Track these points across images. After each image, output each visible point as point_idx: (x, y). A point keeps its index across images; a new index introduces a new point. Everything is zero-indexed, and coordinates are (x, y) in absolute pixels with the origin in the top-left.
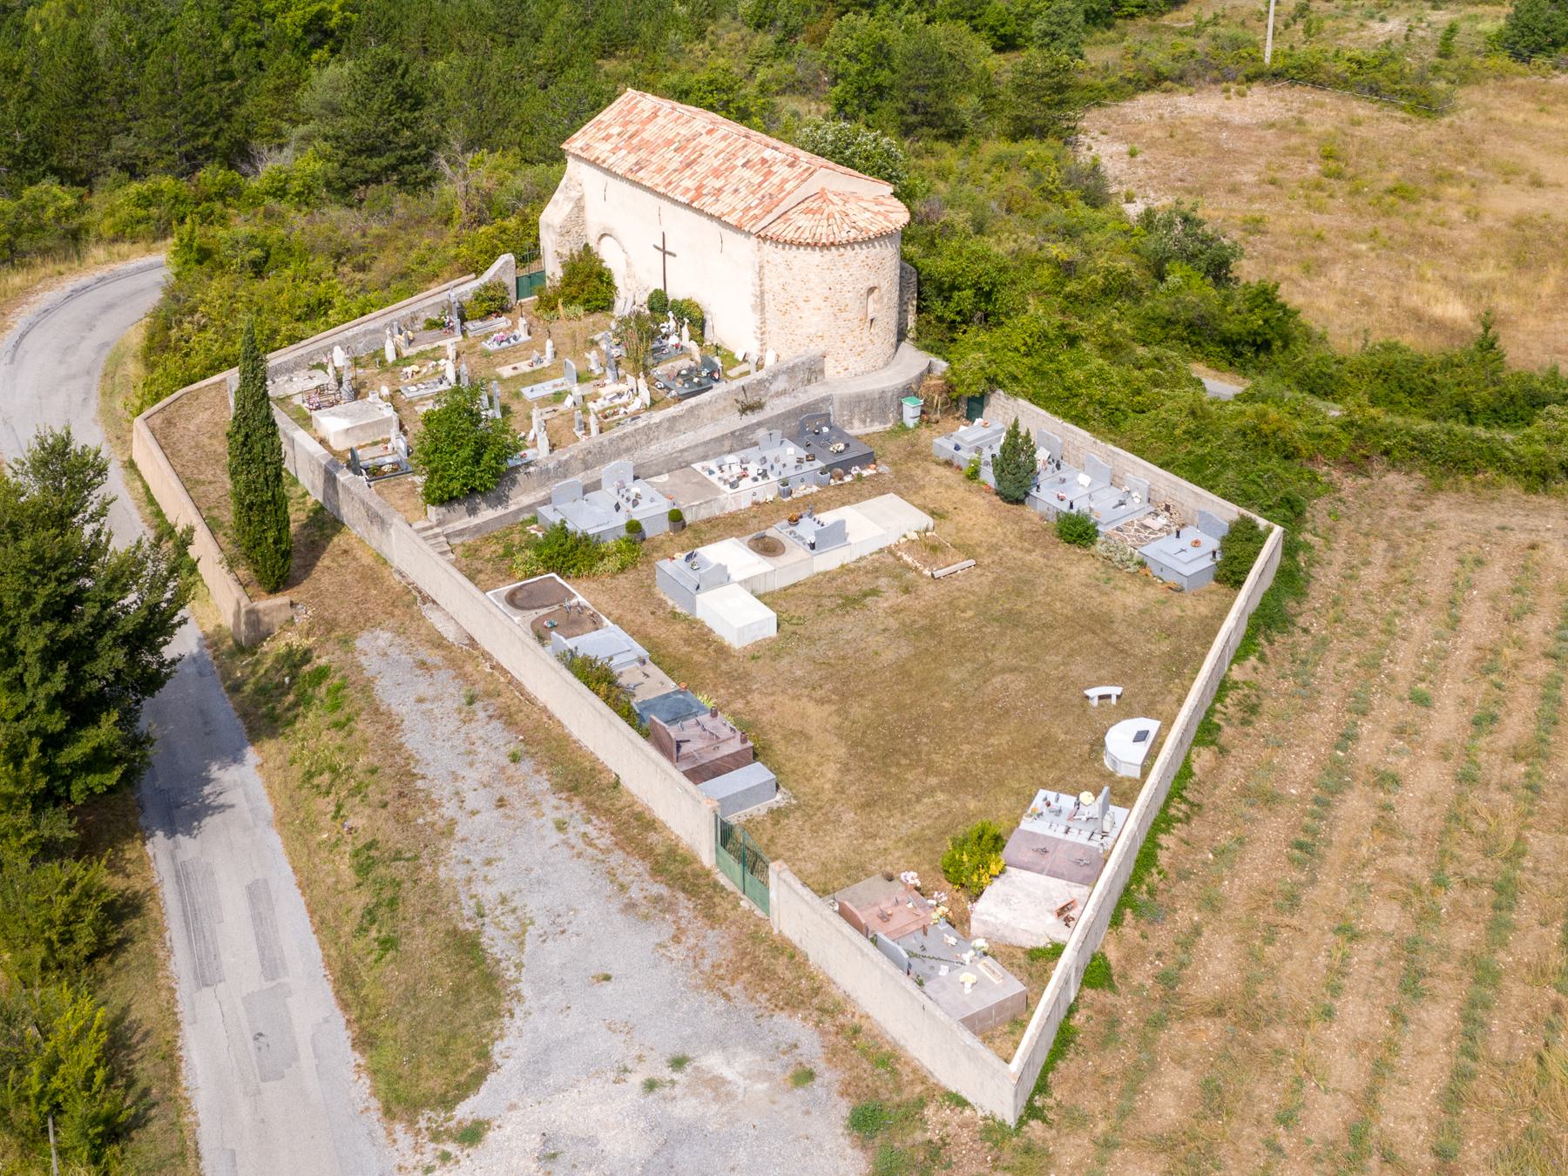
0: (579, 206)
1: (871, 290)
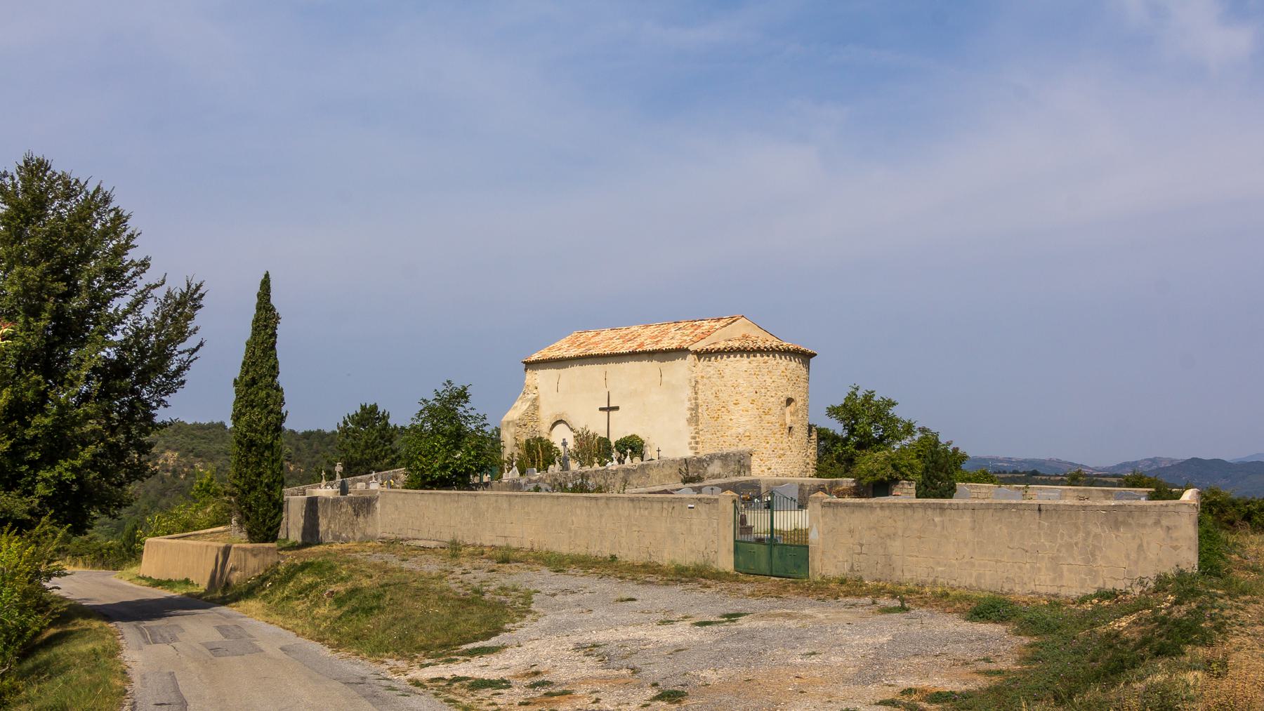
0: (535, 405)
1: (789, 401)
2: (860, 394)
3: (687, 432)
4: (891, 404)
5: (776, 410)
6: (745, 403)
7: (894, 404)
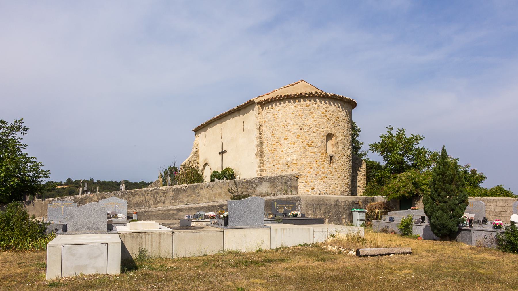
1: (330, 136)
2: (395, 133)
3: (256, 162)
4: (418, 139)
5: (318, 143)
6: (292, 138)
7: (421, 139)
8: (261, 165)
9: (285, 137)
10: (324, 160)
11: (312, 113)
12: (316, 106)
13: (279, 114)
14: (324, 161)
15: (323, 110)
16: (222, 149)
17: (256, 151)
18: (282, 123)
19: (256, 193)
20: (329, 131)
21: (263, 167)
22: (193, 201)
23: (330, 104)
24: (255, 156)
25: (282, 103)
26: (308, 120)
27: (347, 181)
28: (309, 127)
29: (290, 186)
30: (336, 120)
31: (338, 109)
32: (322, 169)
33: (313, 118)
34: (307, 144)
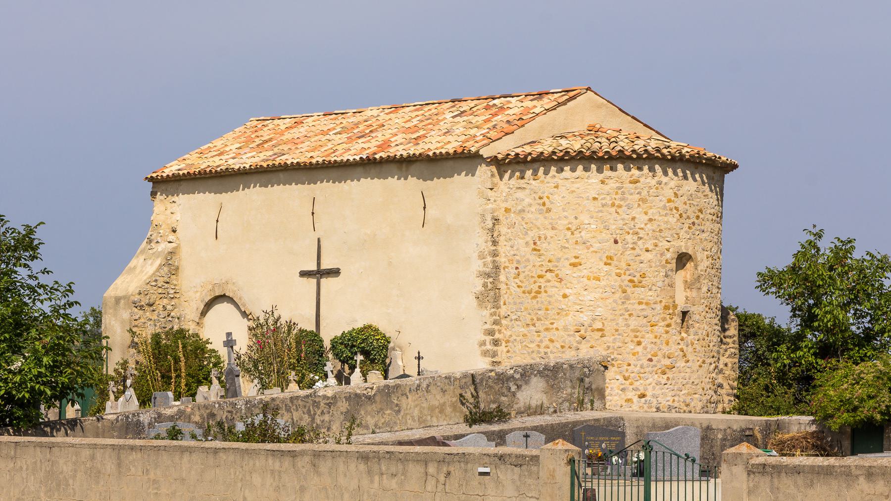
0: (171, 265)
1: (683, 260)
2: (826, 245)
3: (479, 321)
5: (656, 277)
6: (593, 263)
8: (496, 327)
9: (574, 260)
10: (669, 321)
11: (644, 200)
12: (653, 182)
13: (556, 198)
14: (668, 326)
15: (670, 194)
16: (319, 264)
17: (479, 288)
18: (565, 222)
19: (516, 406)
20: (683, 246)
21: (500, 332)
22: (387, 424)
23: (685, 177)
24: (475, 303)
25: (567, 168)
26: (633, 219)
27: (714, 375)
28: (635, 237)
29: (589, 389)
30: (698, 217)
31: (701, 187)
32: (664, 347)
33: (646, 213)
34: (631, 281)
